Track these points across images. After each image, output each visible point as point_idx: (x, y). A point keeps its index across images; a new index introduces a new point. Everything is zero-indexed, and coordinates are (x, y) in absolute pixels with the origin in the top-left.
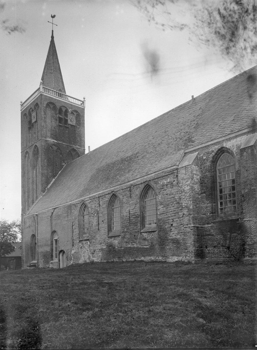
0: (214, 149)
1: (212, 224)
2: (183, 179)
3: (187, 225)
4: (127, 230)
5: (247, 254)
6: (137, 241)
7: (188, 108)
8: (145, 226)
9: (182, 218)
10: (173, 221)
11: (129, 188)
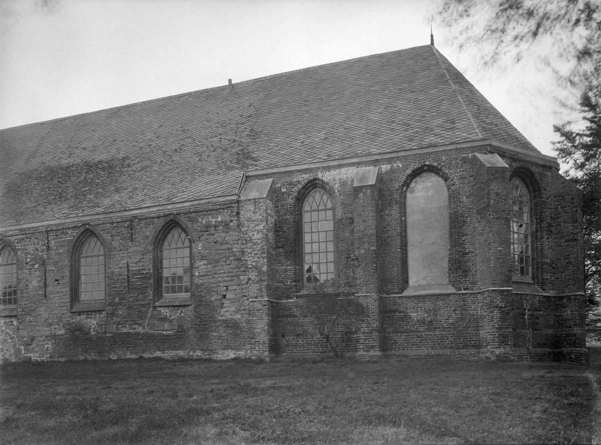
0: (301, 179)
1: (295, 298)
2: (249, 220)
3: (256, 298)
4: (120, 300)
5: (361, 347)
6: (144, 322)
7: (223, 99)
8: (162, 296)
9: (245, 286)
10: (227, 289)
11: (128, 223)
